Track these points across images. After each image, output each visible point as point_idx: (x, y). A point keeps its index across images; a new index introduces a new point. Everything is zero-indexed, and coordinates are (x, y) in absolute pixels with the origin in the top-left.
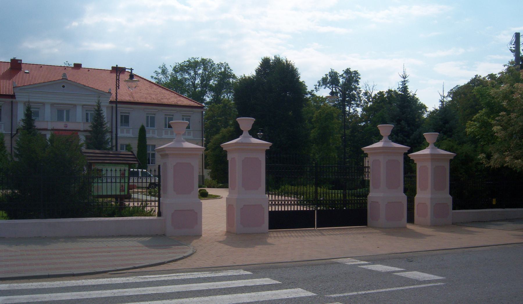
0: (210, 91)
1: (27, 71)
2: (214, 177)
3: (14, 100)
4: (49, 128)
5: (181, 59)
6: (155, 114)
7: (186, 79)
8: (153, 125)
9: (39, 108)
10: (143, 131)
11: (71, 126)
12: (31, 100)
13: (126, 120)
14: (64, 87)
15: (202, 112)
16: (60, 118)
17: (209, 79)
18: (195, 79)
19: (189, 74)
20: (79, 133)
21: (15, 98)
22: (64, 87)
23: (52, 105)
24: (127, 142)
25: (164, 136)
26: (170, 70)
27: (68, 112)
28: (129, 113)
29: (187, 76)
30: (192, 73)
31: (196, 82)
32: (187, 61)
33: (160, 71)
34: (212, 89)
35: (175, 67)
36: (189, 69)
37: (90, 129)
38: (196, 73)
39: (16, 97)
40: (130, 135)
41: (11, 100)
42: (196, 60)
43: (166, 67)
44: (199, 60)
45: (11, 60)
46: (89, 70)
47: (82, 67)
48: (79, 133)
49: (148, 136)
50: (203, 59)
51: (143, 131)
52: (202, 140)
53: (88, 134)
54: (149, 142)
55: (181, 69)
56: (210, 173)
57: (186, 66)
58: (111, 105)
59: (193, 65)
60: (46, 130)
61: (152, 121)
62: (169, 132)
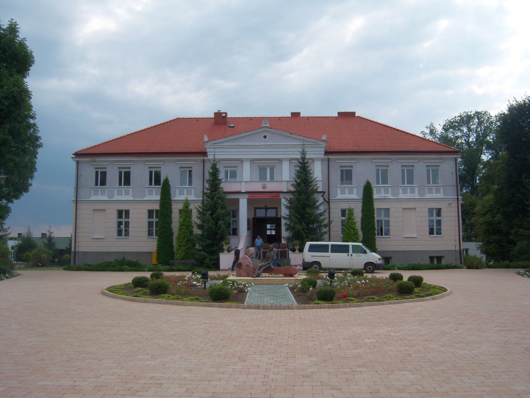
0: (487, 149)
1: (233, 125)
2: (490, 255)
3: (206, 158)
4: (243, 191)
5: (454, 114)
6: (388, 166)
7: (457, 138)
8: (385, 181)
9: (236, 167)
10: (368, 190)
11: (271, 187)
12: (217, 157)
13: (347, 176)
14: (265, 137)
15: (456, 159)
16: (262, 177)
17: (485, 135)
18: (469, 136)
19: (461, 131)
20: (281, 196)
21: (207, 156)
22: (265, 137)
23: (252, 161)
24: (346, 206)
25: (402, 196)
26: (439, 129)
27: (272, 170)
28: (352, 166)
29: (459, 134)
30: (465, 130)
31: (471, 140)
32: (459, 116)
33: (427, 131)
34: (489, 146)
35: (444, 126)
36: (461, 126)
37: (292, 189)
38: (470, 130)
39: (208, 154)
40: (354, 196)
41: (202, 158)
42: (469, 114)
43: (435, 126)
44: (473, 112)
45: (215, 113)
46: (308, 118)
47: (301, 116)
48: (281, 196)
49: (375, 196)
50: (477, 112)
51: (368, 190)
52: (458, 198)
53: (290, 196)
54: (377, 205)
55: (451, 126)
56: (481, 247)
57: (456, 122)
58: (326, 157)
59: (466, 120)
60: (239, 193)
61: (384, 177)
62: (409, 190)
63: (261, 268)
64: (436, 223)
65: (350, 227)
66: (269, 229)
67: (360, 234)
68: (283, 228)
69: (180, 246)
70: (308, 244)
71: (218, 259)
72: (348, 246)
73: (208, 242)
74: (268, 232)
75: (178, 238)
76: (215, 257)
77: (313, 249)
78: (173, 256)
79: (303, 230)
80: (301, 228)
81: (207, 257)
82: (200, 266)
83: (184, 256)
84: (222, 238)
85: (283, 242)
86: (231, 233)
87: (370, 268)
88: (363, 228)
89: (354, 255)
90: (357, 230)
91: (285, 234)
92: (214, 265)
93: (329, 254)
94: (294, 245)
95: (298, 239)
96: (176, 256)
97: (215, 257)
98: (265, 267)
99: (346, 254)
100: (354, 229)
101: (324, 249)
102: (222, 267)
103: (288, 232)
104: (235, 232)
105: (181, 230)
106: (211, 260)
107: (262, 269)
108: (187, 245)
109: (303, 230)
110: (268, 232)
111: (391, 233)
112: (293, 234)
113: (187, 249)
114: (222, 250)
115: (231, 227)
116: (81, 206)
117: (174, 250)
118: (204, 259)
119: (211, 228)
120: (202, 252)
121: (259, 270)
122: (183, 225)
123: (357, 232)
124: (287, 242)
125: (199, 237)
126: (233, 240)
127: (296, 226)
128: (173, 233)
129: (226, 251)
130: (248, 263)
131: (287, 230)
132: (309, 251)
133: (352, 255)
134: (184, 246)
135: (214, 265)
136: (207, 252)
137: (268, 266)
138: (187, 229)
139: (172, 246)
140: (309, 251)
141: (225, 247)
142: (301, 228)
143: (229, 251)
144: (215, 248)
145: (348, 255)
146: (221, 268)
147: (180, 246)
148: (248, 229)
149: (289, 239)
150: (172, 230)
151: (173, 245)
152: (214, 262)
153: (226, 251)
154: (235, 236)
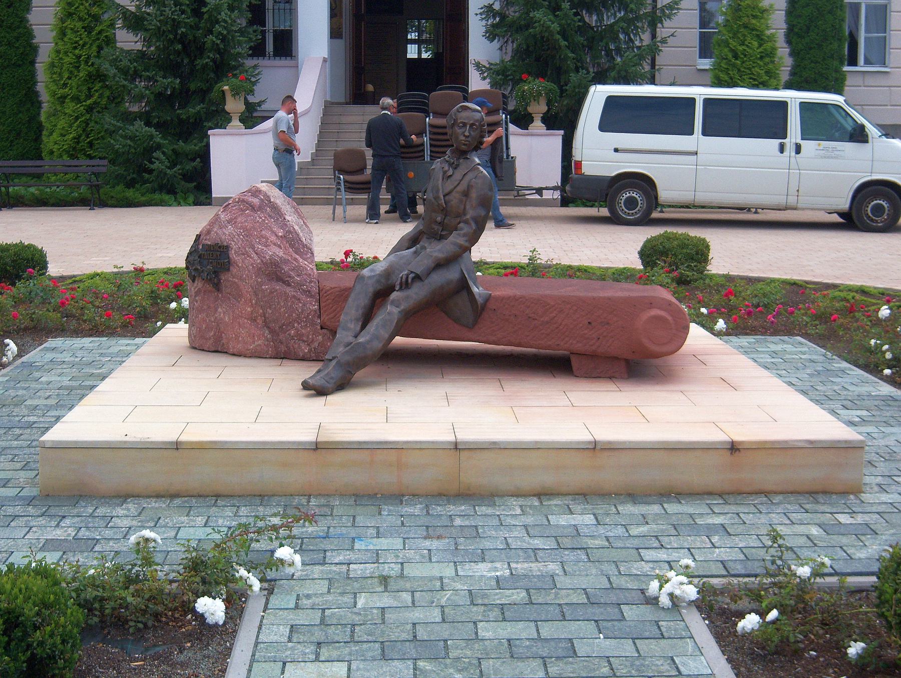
63: (381, 294)
64: (865, 41)
65: (745, 26)
66: (413, 42)
67: (783, 52)
68: (476, 27)
69: (62, 99)
70: (598, 95)
71: (204, 156)
72: (782, 106)
73: (169, 83)
74: (412, 52)
75: (52, 65)
76: (192, 147)
77: (618, 116)
78: (38, 139)
79: (564, 34)
80: (555, 27)
81: (159, 147)
82: (130, 184)
83: (77, 140)
84: (223, 67)
85: (477, 82)
86: (270, 47)
87: (878, 210)
88: (791, 35)
89: (809, 146)
90: (771, 38)
91: (481, 48)
92: (187, 177)
93: (696, 140)
94: (525, 99)
95: (541, 75)
96: (49, 142)
97: (192, 147)
98: (418, 293)
99: (776, 142)
100: (760, 38)
101: (671, 116)
102: (219, 189)
103: (496, 44)
104: (285, 45)
105: (62, 33)
106: (176, 158)
107: (391, 311)
108: (89, 96)
109: (564, 34)
110: (412, 52)
111: (895, 56)
112: (516, 52)
113: (90, 109)
114: (221, 119)
115: (270, 26)
116: (799, 205)
117: (43, 118)
118: (149, 152)
119: (176, 24)
120: (139, 124)
121: (367, 318)
122: (70, 15)
123: (774, 49)
124: (494, 84)
125: (125, 63)
126: (269, 76)
127: (538, 15)
128: (35, 49)
129: (236, 122)
130: (276, 252)
131: (491, 34)
132: (606, 125)
133: (798, 149)
134: (76, 99)
135: (187, 177)
136: (158, 126)
137: (439, 278)
138: (88, 29)
139: (31, 98)
140: (606, 125)
141: (234, 106)
142: (555, 27)
143: (252, 117)
144: (195, 109)
145: (782, 149)
146: (214, 195)
147: (62, 99)
148: (335, 33)
149: (500, 75)
150: (29, 35)
151: (37, 94)
152: (189, 166)
153: (236, 122)
154: (283, 62)
